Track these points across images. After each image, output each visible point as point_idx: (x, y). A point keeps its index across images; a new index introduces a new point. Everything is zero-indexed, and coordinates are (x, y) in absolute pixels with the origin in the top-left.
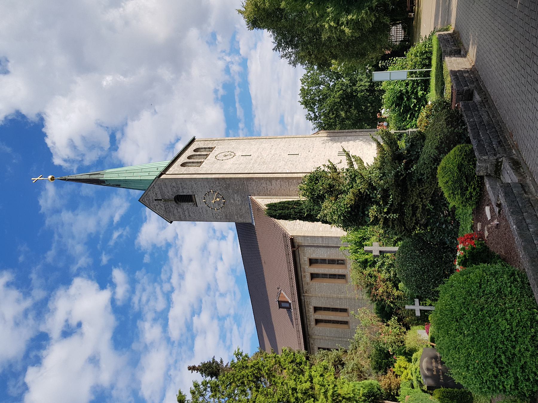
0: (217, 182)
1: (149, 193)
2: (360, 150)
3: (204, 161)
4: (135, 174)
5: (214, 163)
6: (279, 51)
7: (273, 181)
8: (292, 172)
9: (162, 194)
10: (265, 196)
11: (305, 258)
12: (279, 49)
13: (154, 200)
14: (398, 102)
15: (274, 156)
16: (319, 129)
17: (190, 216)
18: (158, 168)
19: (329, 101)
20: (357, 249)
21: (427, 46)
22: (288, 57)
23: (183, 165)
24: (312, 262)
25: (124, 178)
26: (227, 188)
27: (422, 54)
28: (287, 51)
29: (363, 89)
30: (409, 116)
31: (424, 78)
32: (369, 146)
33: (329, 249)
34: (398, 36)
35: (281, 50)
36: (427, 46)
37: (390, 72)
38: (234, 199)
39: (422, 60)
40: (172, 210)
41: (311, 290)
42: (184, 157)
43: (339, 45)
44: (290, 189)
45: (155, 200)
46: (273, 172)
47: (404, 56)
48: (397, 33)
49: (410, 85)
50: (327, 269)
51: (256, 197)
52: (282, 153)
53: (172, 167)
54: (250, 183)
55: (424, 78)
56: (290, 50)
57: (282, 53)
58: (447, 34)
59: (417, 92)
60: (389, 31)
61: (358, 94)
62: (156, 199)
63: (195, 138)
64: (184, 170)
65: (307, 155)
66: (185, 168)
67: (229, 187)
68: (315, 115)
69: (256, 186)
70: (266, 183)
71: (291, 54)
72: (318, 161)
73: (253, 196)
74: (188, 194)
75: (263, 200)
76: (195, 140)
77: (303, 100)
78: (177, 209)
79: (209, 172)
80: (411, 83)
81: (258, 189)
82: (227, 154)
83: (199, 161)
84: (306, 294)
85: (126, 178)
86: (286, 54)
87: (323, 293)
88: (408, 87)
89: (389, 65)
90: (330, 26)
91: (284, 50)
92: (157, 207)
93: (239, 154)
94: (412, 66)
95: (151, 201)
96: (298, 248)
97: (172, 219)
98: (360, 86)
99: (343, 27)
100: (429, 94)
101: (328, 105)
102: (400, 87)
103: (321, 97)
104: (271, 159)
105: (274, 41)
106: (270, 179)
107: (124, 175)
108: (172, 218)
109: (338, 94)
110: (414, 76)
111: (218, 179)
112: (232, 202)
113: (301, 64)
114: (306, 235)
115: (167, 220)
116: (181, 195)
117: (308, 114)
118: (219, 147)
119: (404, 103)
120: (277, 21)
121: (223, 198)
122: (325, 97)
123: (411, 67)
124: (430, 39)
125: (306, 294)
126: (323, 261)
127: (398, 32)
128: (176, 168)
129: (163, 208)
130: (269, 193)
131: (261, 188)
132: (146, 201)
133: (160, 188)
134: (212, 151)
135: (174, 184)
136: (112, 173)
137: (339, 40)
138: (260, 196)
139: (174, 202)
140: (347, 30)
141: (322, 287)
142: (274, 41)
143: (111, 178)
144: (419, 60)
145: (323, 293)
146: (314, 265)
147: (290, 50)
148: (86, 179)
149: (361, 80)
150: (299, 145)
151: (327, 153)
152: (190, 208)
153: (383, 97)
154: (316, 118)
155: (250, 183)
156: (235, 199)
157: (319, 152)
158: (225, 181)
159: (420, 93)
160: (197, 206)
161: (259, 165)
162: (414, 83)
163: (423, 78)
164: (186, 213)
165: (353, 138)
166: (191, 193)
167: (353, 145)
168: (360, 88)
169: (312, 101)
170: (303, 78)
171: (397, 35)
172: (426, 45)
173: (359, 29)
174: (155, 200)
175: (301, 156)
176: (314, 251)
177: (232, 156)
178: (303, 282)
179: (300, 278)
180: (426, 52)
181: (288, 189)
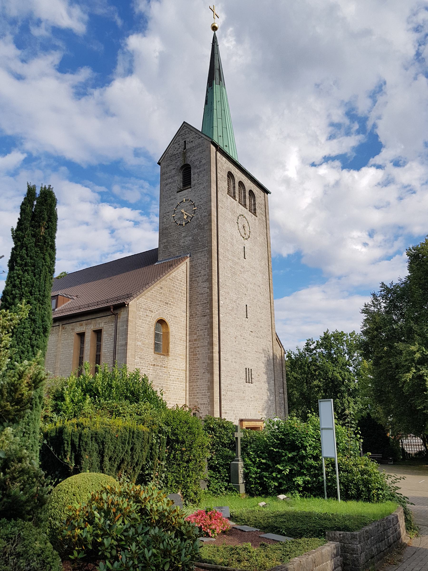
0: (206, 213)
1: (193, 133)
2: (254, 397)
3: (236, 200)
4: (219, 120)
5: (234, 212)
6: (381, 292)
7: (208, 283)
8: (220, 308)
9: (192, 149)
10: (190, 275)
11: (103, 323)
12: (383, 291)
13: (184, 140)
14: (287, 443)
15: (244, 287)
16: (297, 355)
17: (167, 185)
18: (228, 147)
19: (329, 365)
20: (82, 386)
21: (380, 492)
22: (373, 303)
23: (230, 175)
24: (98, 333)
25: (215, 108)
26: (199, 226)
27: (366, 483)
28: (381, 300)
29: (345, 405)
30: (264, 461)
31: (325, 486)
32: (260, 409)
33: (112, 354)
34: (413, 446)
35: (382, 293)
36: (380, 492)
37: (332, 429)
38: (186, 237)
39: (355, 484)
40: (174, 162)
41: (66, 335)
42: (242, 177)
43: (391, 367)
44: (198, 306)
45: (185, 142)
46: (220, 284)
47: (365, 451)
48: (416, 445)
49: (314, 463)
50: (89, 353)
51: (188, 263)
52: (249, 298)
53: (227, 161)
54: (205, 255)
55: (325, 486)
56: (383, 305)
57: (379, 295)
58: (399, 533)
59: (302, 474)
60: (417, 435)
61: (339, 399)
62: (187, 142)
63: (269, 194)
64: (223, 176)
65: (246, 328)
66: (226, 177)
67: (201, 229)
68: (313, 349)
69: (202, 263)
70: (205, 275)
71: (379, 307)
72: (237, 342)
73: (190, 259)
74: (192, 180)
75: (184, 272)
76: (265, 194)
77: (330, 334)
78: (174, 169)
79: (219, 205)
80: (318, 464)
81: (198, 265)
82: (246, 229)
83: (236, 195)
84: (61, 327)
85: (215, 111)
86: (378, 300)
87: (61, 350)
88: (311, 459)
89: (348, 426)
90: (415, 353)
91: (383, 297)
92: (177, 144)
93: (247, 244)
94: (347, 465)
95: (184, 137)
96: (113, 314)
97: (163, 164)
98: (348, 401)
99: (414, 371)
100: (298, 495)
101: (324, 363)
102: (310, 445)
103: (335, 356)
104: (239, 283)
105: (394, 284)
106: (210, 280)
107: (219, 107)
108: (164, 164)
109: (338, 375)
110: (194, 488)
111: (210, 215)
112: (183, 235)
113: (365, 320)
114: (130, 323)
115: (162, 158)
116: (191, 172)
117: (314, 341)
118: (257, 221)
119: (286, 454)
120: (420, 284)
121: (187, 223)
122: (334, 361)
123: (344, 464)
124: (392, 497)
125: (61, 327)
126: (99, 348)
127: (417, 447)
128: (226, 165)
129: (175, 152)
130: (193, 279)
131: (200, 269)
132: (183, 131)
133: (199, 145)
134: (251, 212)
135: (204, 161)
136: (221, 94)
137: (397, 367)
138: (190, 268)
139: (182, 164)
140: (409, 375)
141: (69, 348)
142: (393, 285)
143: (215, 93)
144: (355, 478)
145: (61, 350)
146: (95, 336)
147: (383, 305)
148: (214, 66)
149: (355, 403)
150: (260, 320)
151: (249, 354)
152: (175, 185)
153: (295, 418)
154: (308, 349)
155: (205, 255)
156: (186, 238)
157: (251, 344)
158: (207, 224)
159: (299, 480)
160: (178, 192)
161: (231, 267)
162: (317, 470)
163: (325, 484)
164: (170, 180)
165: (272, 388)
166: (193, 183)
167: (261, 389)
168: (346, 402)
169: (329, 345)
170: (356, 334)
171: (414, 445)
172: (382, 489)
173: (414, 392)
174: (185, 142)
175: (245, 321)
176: (111, 335)
177: (244, 235)
178: (75, 323)
179: (80, 319)
180: (369, 491)
181: (198, 303)
